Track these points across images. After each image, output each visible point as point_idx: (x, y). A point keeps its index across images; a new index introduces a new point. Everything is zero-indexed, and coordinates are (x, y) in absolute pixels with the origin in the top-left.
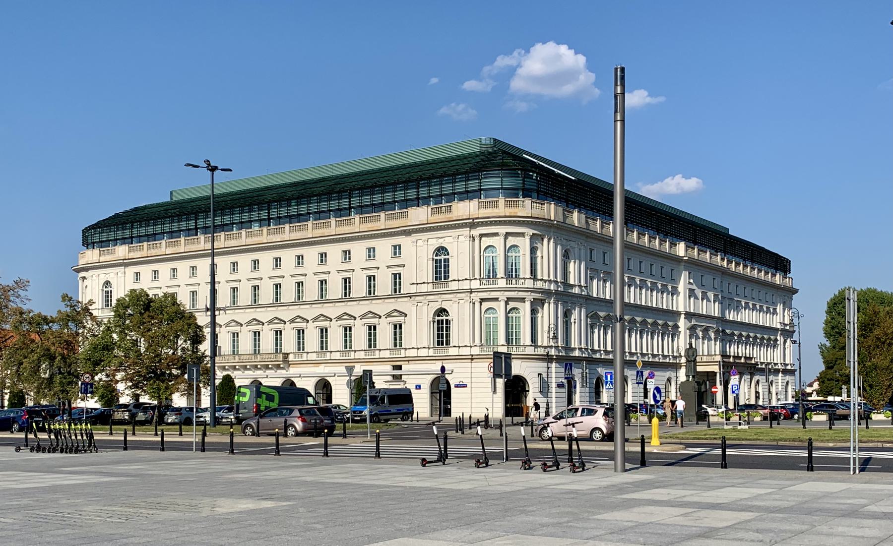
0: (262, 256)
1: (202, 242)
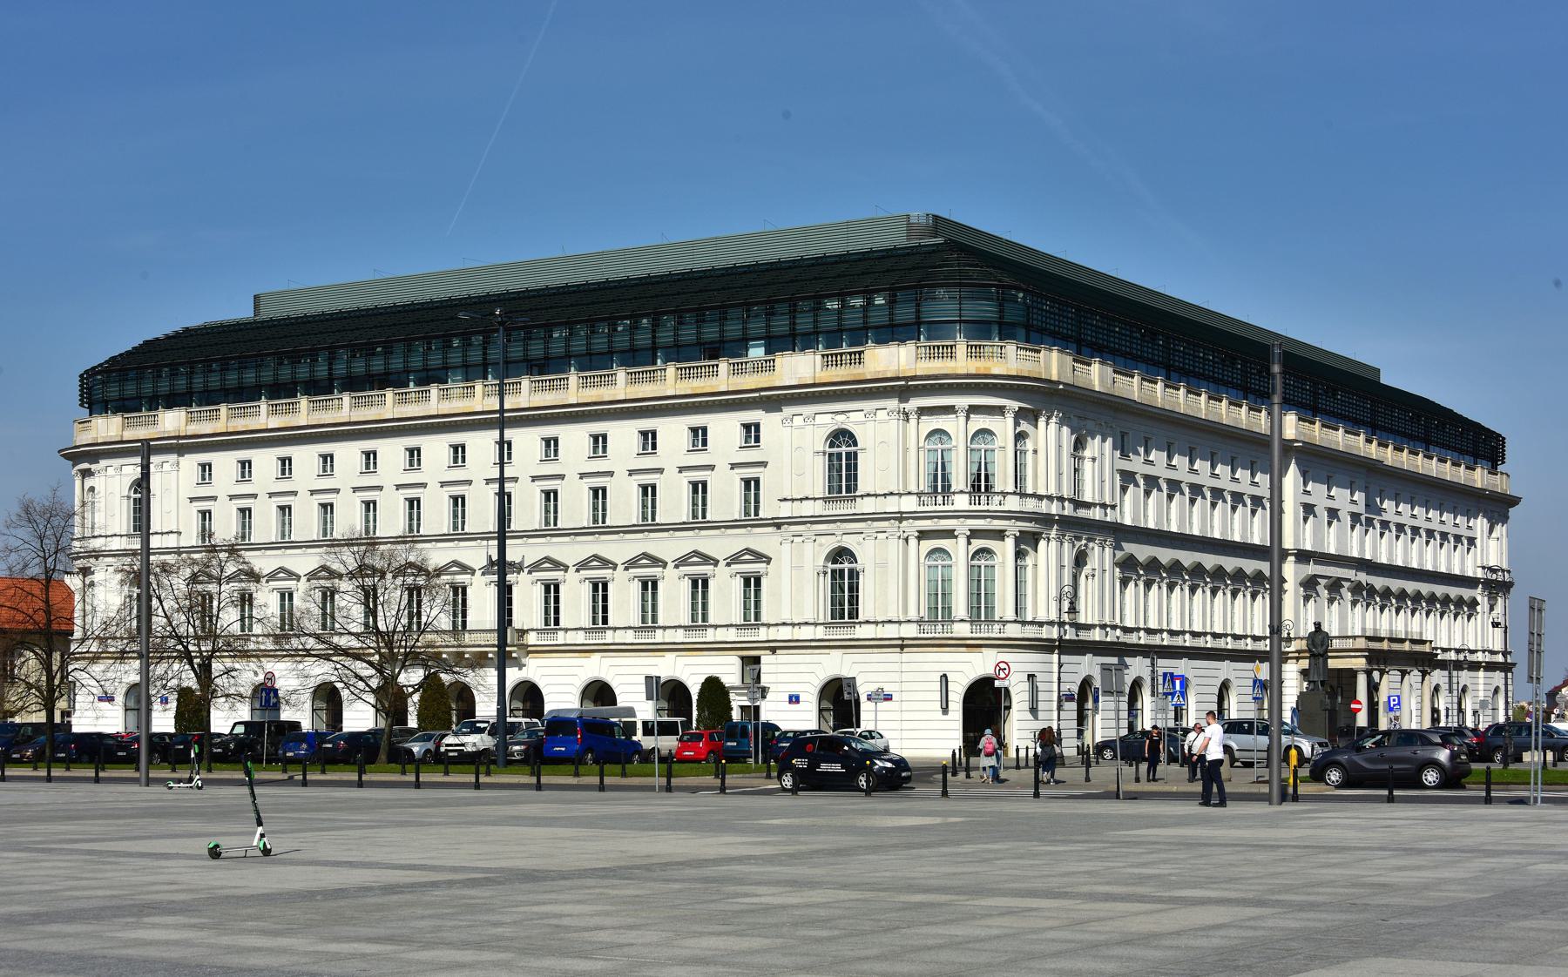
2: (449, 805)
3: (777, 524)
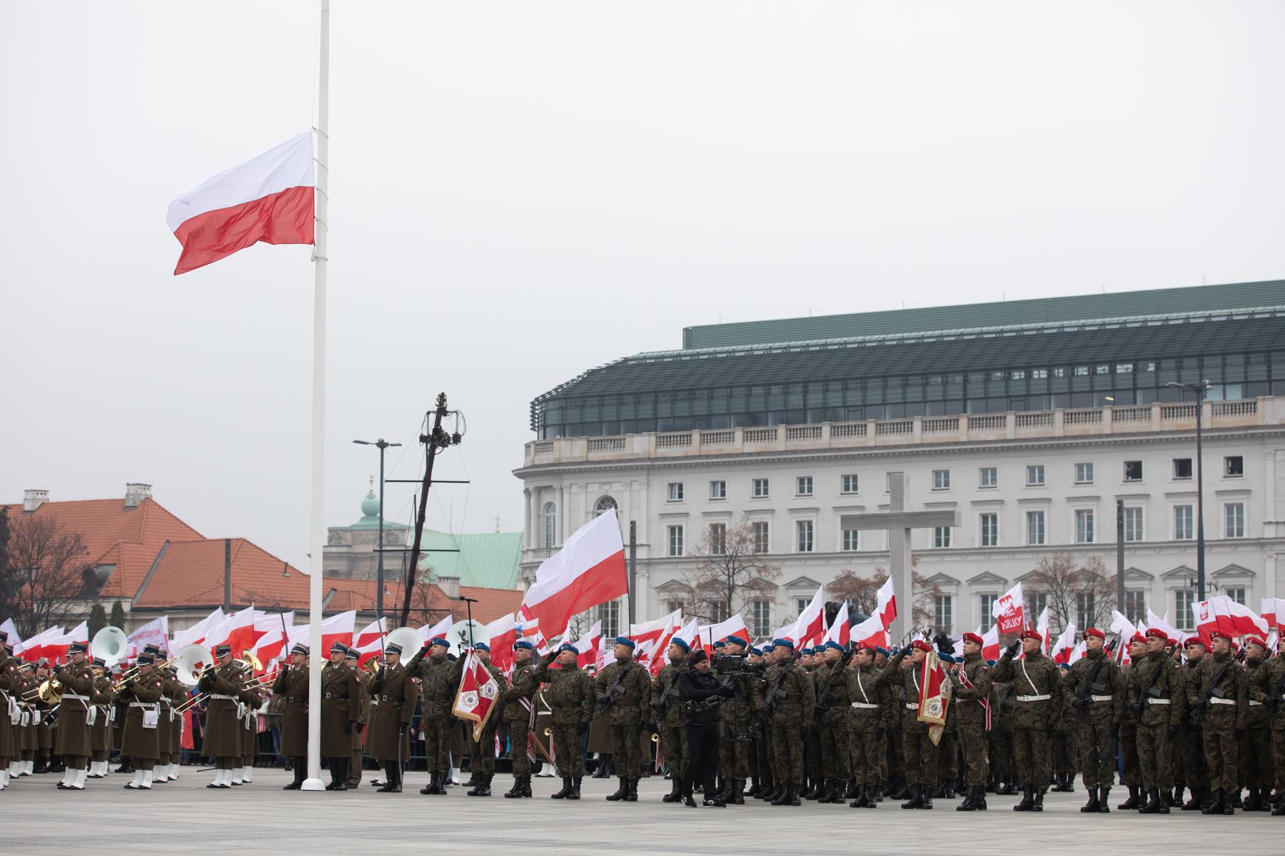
2: (488, 839)
3: (1261, 543)
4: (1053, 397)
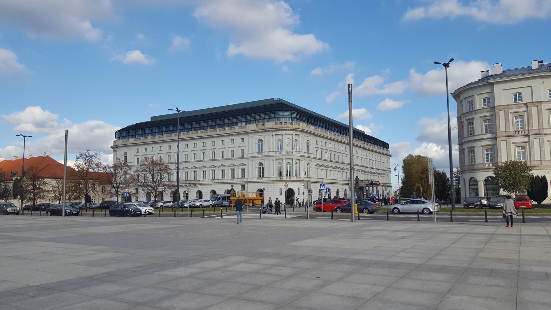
0: (198, 142)
1: (174, 136)
3: (247, 158)
4: (256, 121)
